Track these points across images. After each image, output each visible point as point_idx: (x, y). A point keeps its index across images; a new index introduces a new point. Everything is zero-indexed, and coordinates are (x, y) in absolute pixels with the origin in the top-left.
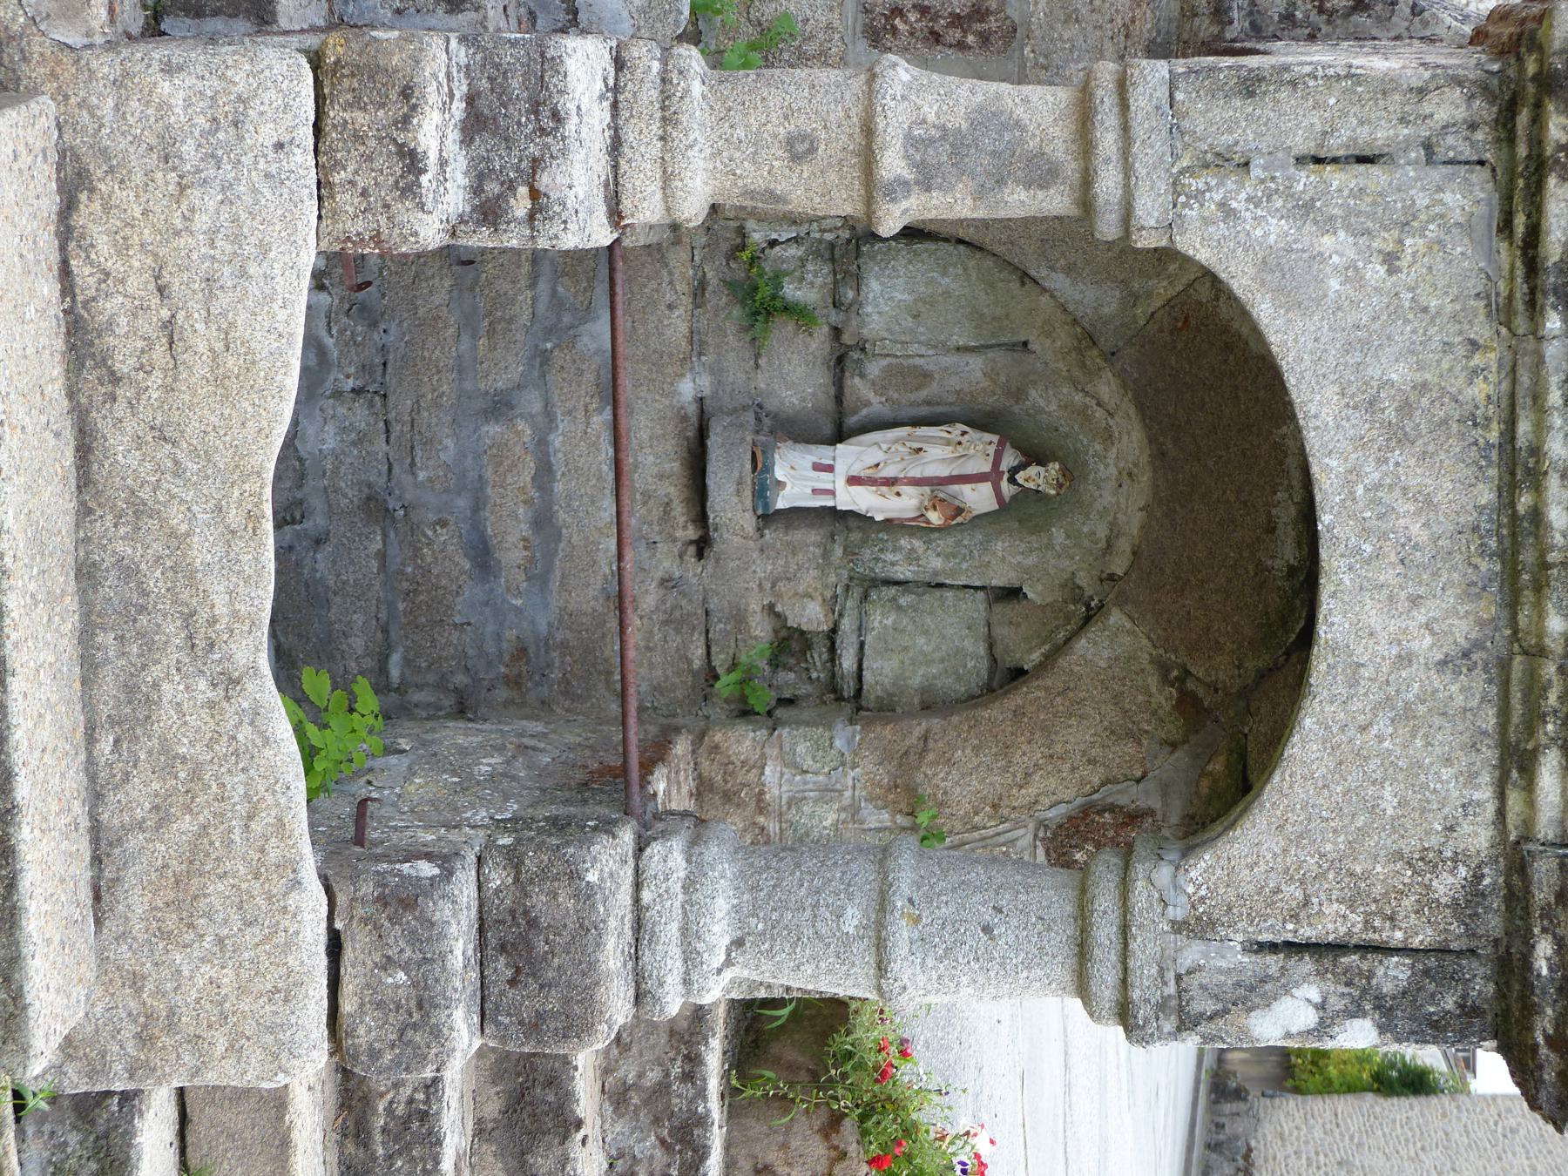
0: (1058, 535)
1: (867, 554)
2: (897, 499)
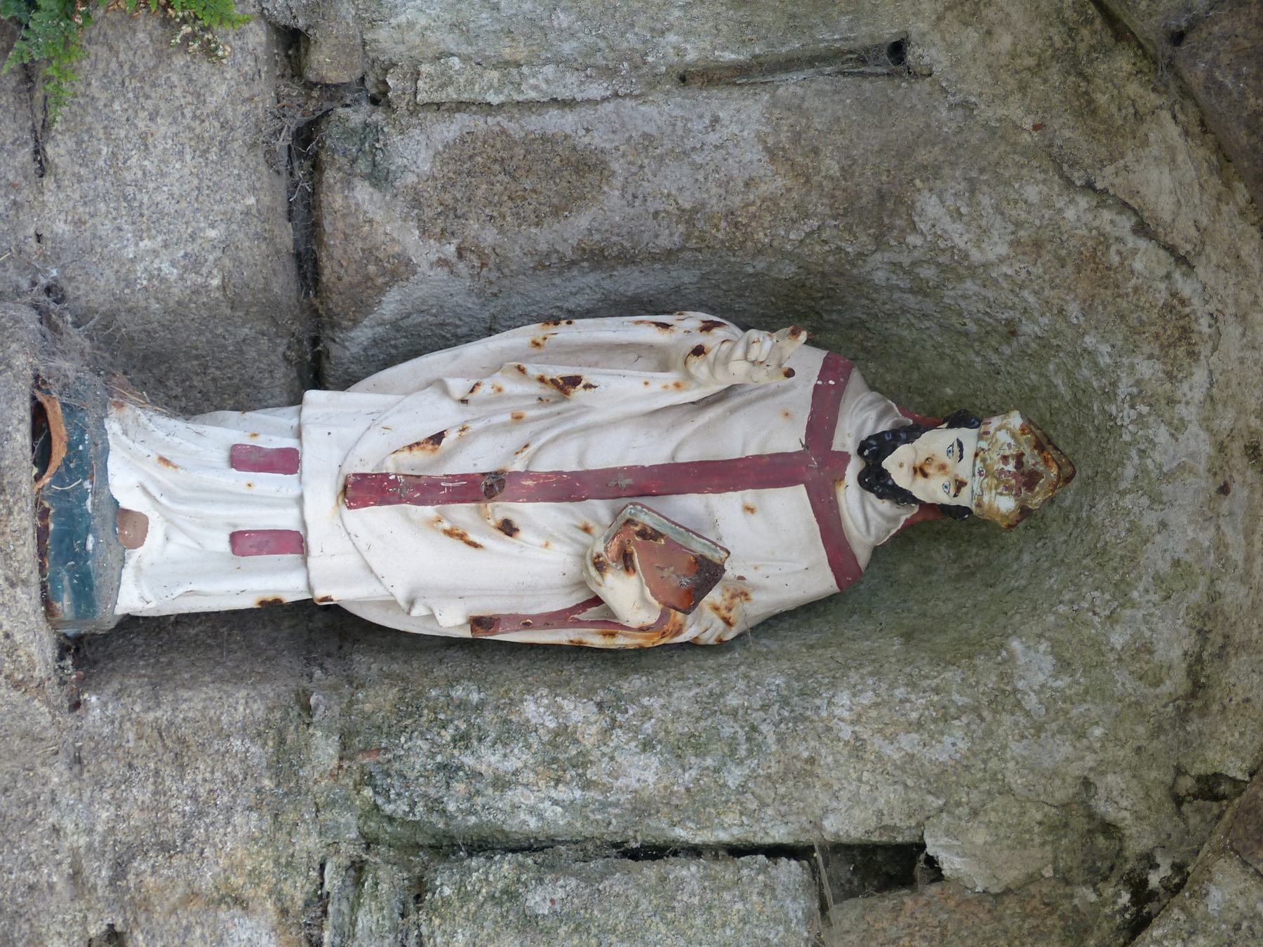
0: (1033, 664)
1: (417, 753)
2: (497, 543)
